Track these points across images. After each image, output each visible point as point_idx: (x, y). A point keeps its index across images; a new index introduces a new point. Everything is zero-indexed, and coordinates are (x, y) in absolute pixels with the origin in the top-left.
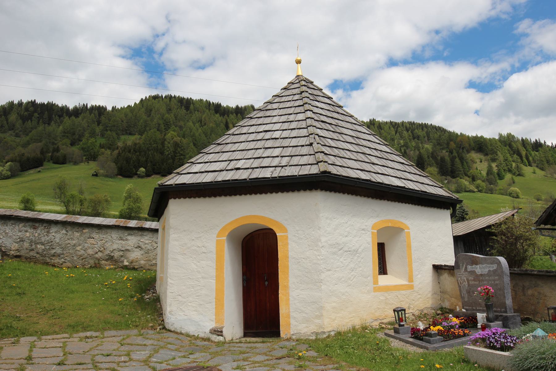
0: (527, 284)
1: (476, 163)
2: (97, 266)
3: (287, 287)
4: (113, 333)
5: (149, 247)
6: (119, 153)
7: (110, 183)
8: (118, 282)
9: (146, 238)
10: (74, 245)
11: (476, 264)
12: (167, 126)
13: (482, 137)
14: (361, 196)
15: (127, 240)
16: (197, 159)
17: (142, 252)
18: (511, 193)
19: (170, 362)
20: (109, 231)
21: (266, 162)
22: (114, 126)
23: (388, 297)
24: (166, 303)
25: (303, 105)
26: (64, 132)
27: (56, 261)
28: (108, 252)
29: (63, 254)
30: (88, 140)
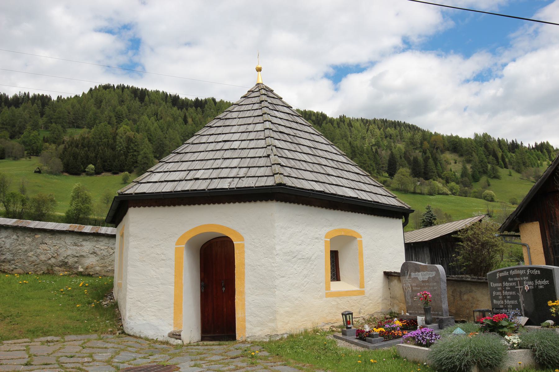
0: (463, 289)
1: (450, 164)
2: (50, 272)
3: (243, 293)
4: (73, 337)
5: (105, 253)
6: (65, 148)
7: (54, 181)
8: (73, 289)
9: (102, 244)
10: (26, 251)
11: (419, 272)
12: (120, 118)
13: (457, 137)
14: (315, 206)
15: (81, 246)
16: (157, 169)
17: (97, 258)
18: (486, 197)
19: (132, 362)
20: (63, 236)
21: (224, 173)
22: (60, 118)
23: (340, 302)
24: (125, 308)
25: (262, 115)
26: (3, 124)
27: (6, 267)
28: (61, 258)
29: (13, 260)
30: (30, 132)
